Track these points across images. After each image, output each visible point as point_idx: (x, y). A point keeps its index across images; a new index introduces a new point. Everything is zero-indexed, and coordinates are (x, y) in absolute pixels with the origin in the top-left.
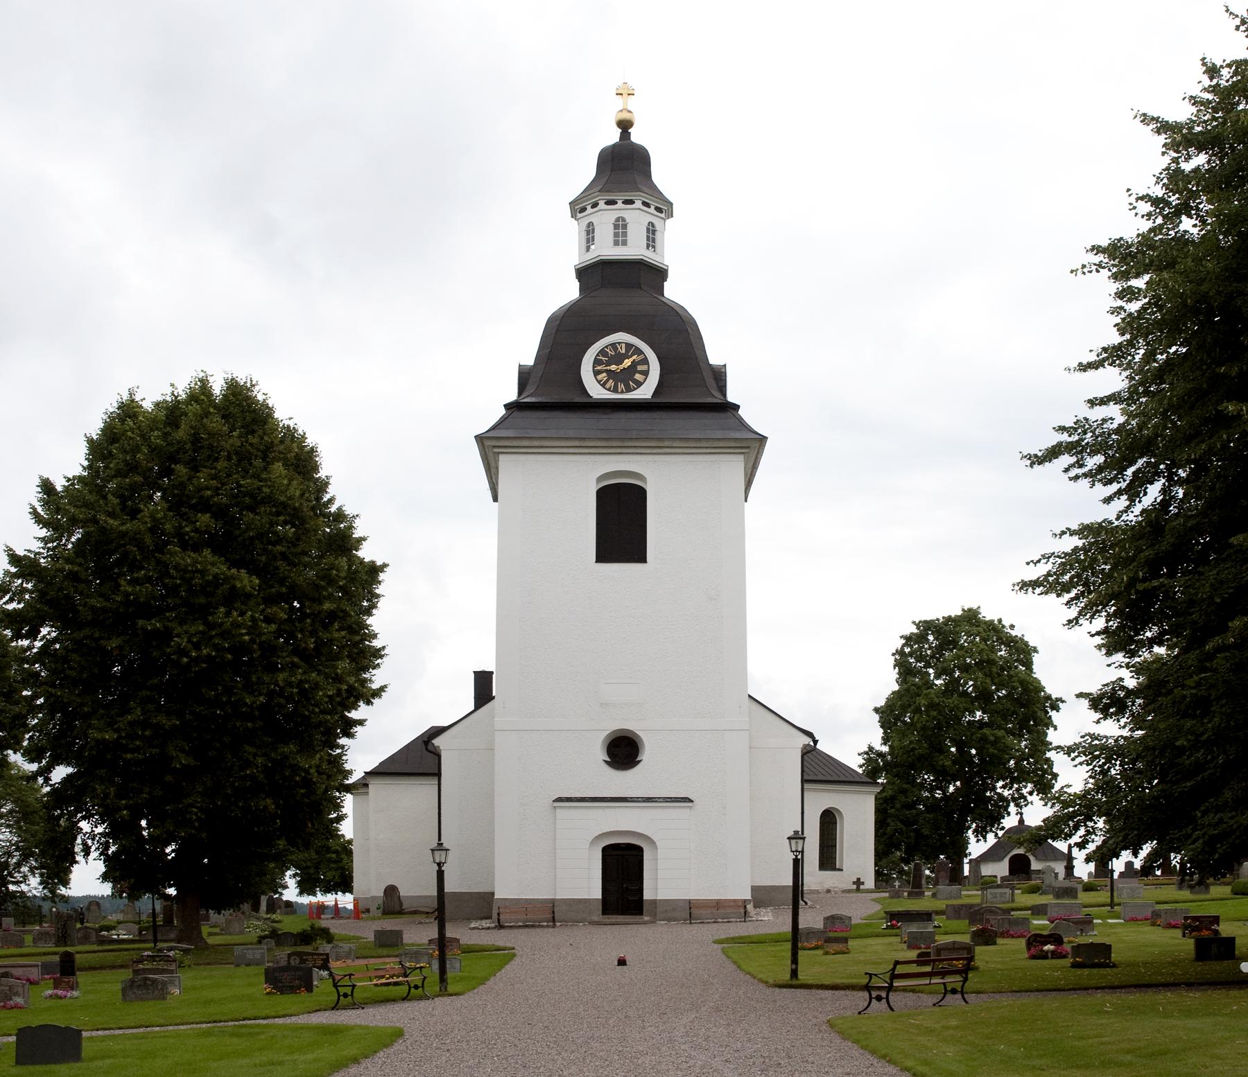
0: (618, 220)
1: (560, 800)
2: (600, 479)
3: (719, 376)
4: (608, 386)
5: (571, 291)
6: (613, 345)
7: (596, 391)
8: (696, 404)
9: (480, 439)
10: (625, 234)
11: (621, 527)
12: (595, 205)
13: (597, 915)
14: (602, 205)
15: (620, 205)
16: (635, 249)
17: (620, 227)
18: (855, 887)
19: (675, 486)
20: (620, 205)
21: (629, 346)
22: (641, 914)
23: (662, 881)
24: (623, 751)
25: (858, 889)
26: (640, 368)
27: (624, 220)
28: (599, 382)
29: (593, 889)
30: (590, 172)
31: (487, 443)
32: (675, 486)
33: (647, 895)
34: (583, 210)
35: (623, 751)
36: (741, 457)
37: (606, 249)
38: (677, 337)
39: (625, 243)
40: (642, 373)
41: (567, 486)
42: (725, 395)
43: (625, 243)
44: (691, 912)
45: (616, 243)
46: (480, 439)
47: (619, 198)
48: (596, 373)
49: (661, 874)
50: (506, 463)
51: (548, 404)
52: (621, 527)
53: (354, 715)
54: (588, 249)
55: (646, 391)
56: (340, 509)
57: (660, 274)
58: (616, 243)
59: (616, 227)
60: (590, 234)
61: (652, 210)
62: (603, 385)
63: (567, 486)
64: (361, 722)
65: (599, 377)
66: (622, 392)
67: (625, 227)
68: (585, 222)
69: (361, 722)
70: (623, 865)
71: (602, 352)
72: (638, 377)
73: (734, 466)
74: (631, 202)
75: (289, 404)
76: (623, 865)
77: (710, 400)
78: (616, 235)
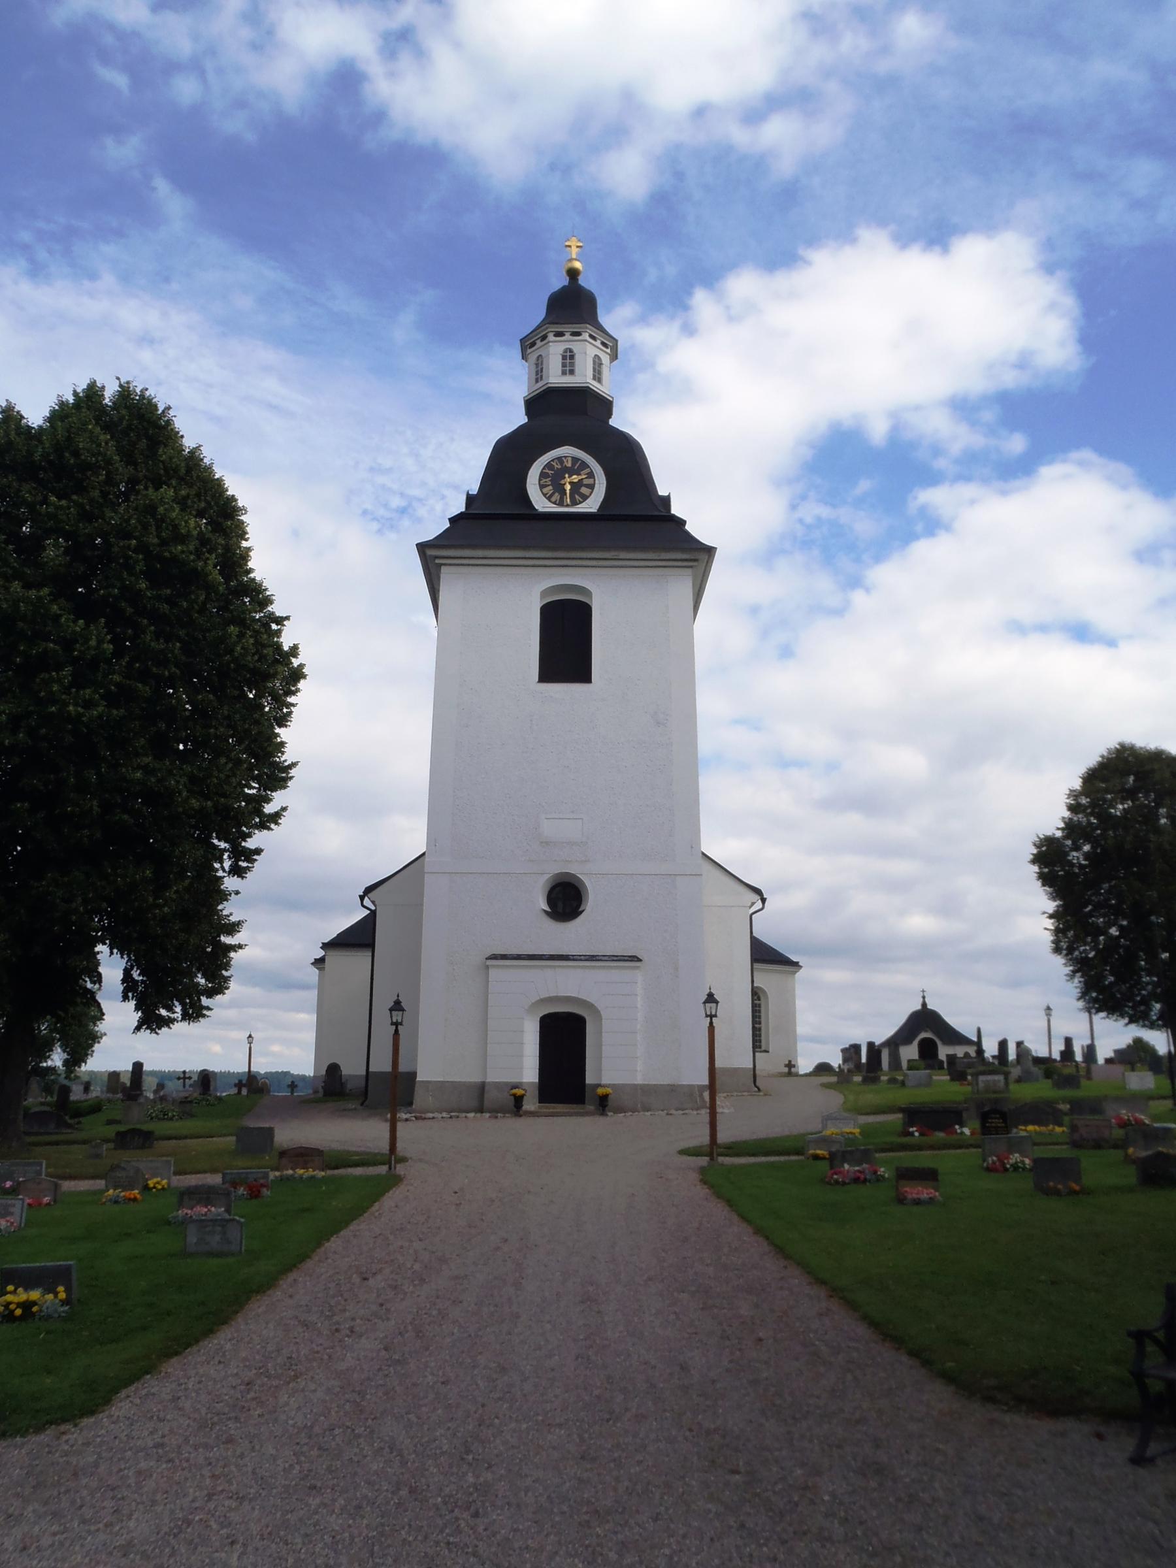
0: (565, 351)
1: (494, 957)
2: (544, 593)
3: (666, 501)
4: (553, 499)
5: (520, 418)
6: (560, 459)
7: (541, 504)
8: (642, 525)
9: (422, 548)
10: (572, 365)
11: (566, 645)
12: (544, 338)
13: (531, 1104)
14: (551, 337)
15: (567, 337)
16: (583, 376)
17: (569, 358)
18: (786, 1070)
19: (620, 602)
20: (567, 337)
21: (575, 460)
22: (583, 1102)
23: (611, 1062)
24: (566, 899)
25: (790, 1074)
26: (586, 482)
27: (571, 351)
28: (545, 495)
29: (529, 1072)
30: (541, 314)
31: (431, 552)
32: (620, 602)
33: (590, 1079)
34: (533, 344)
35: (566, 899)
36: (689, 571)
37: (555, 378)
38: (626, 461)
39: (572, 372)
40: (587, 486)
41: (512, 602)
42: (669, 510)
43: (572, 372)
44: (644, 1099)
45: (564, 373)
46: (422, 548)
47: (568, 328)
48: (542, 487)
49: (606, 1051)
50: (448, 577)
51: (493, 523)
52: (566, 645)
53: (250, 844)
54: (537, 381)
55: (591, 505)
56: (301, 666)
57: (606, 406)
58: (564, 373)
59: (564, 358)
60: (539, 372)
61: (598, 343)
62: (549, 499)
63: (512, 602)
64: (258, 851)
65: (545, 490)
66: (568, 506)
67: (572, 357)
68: (533, 358)
69: (258, 851)
70: (564, 1036)
71: (549, 466)
72: (584, 490)
73: (680, 585)
74: (578, 334)
75: (161, 398)
76: (564, 1036)
77: (656, 513)
78: (564, 365)
